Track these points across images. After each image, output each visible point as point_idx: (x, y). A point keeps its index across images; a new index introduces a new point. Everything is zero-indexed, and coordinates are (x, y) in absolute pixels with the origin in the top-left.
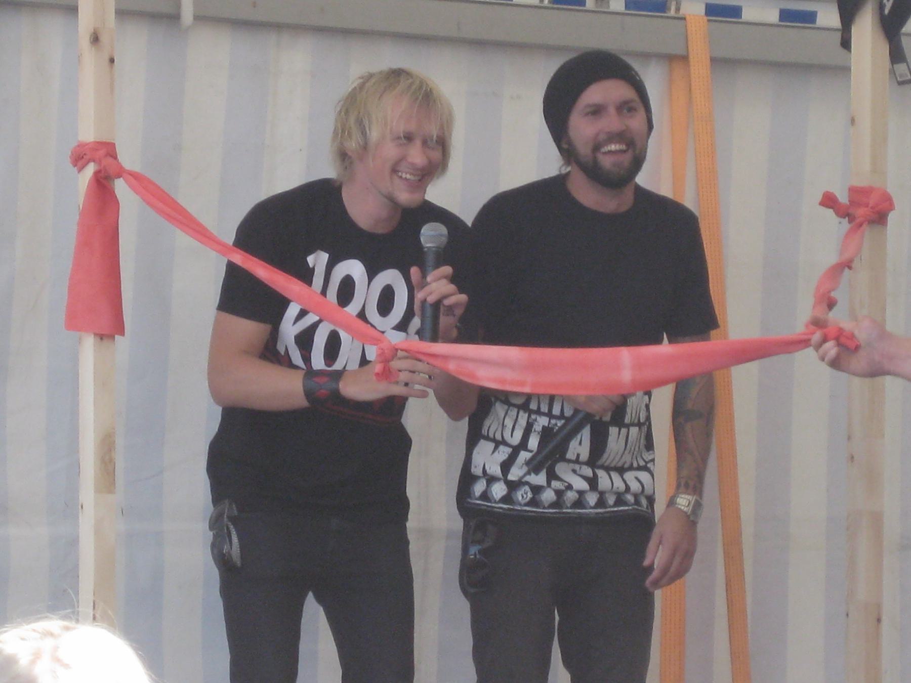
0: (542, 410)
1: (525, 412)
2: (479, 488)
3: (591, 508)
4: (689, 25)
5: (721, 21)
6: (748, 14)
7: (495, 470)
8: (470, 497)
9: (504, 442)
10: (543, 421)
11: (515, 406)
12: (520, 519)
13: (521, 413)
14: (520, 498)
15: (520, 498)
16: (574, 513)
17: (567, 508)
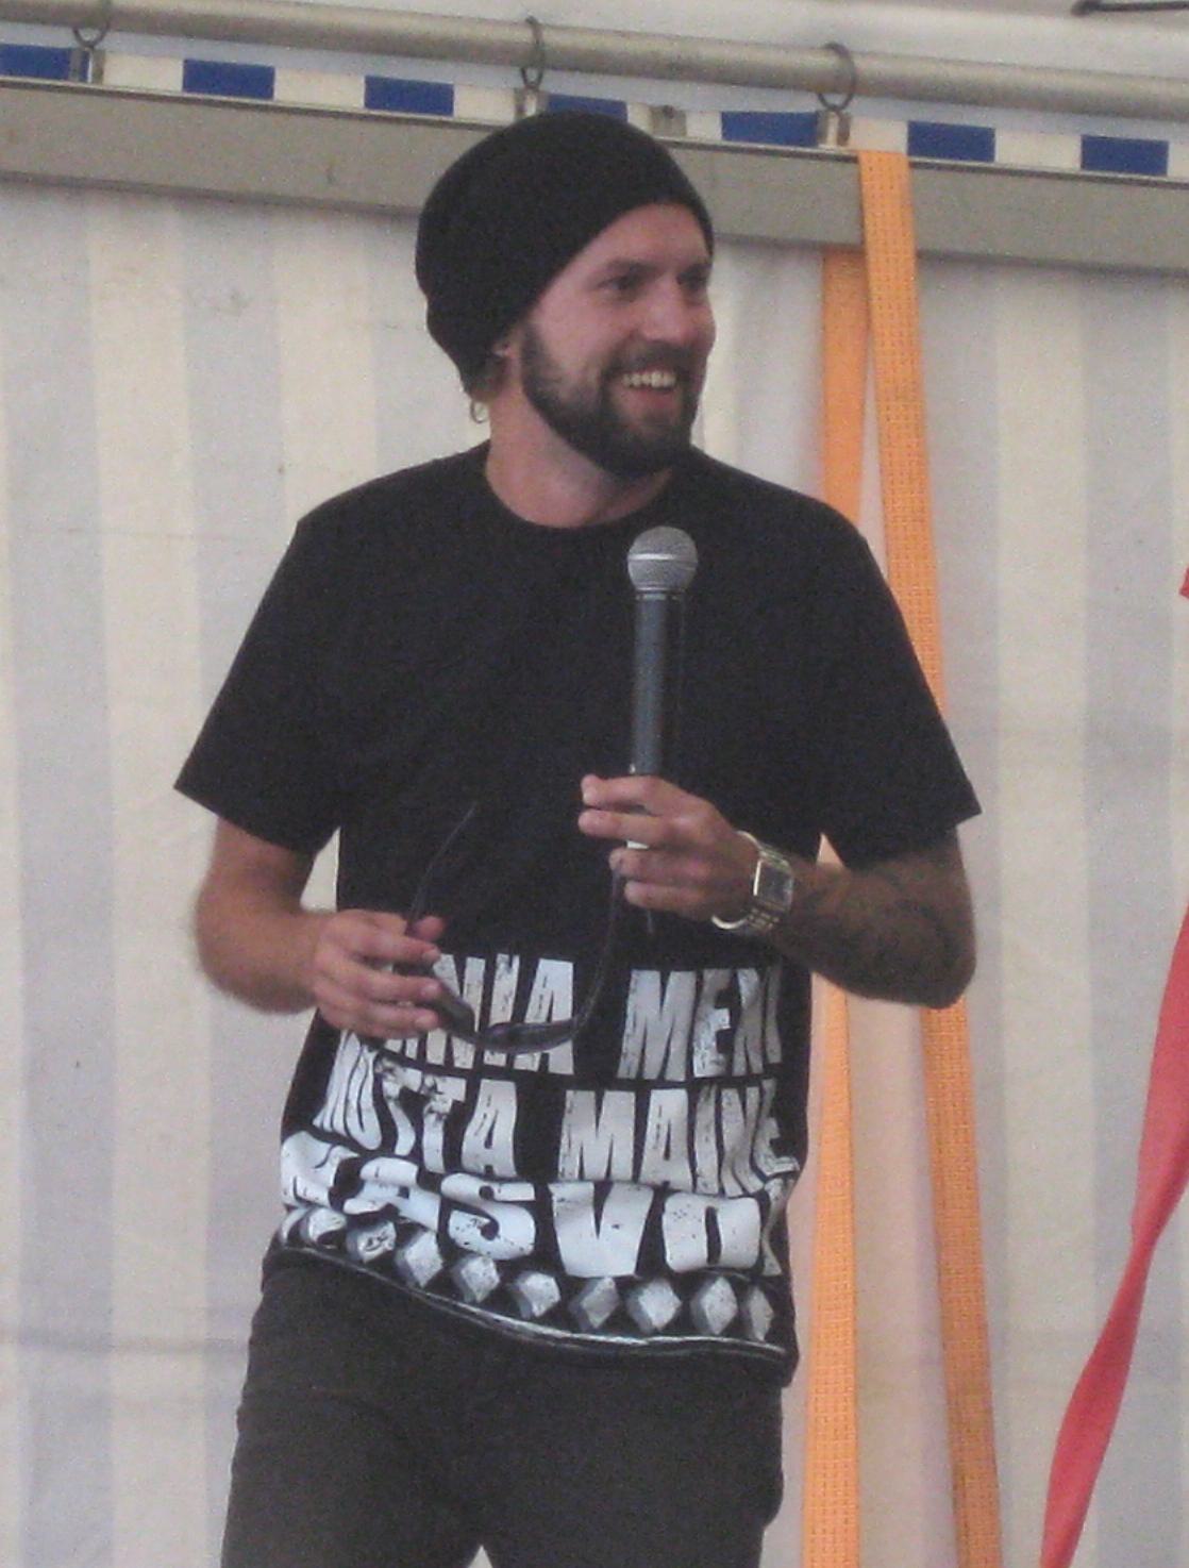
3: (533, 1319)
4: (866, 174)
5: (223, 104)
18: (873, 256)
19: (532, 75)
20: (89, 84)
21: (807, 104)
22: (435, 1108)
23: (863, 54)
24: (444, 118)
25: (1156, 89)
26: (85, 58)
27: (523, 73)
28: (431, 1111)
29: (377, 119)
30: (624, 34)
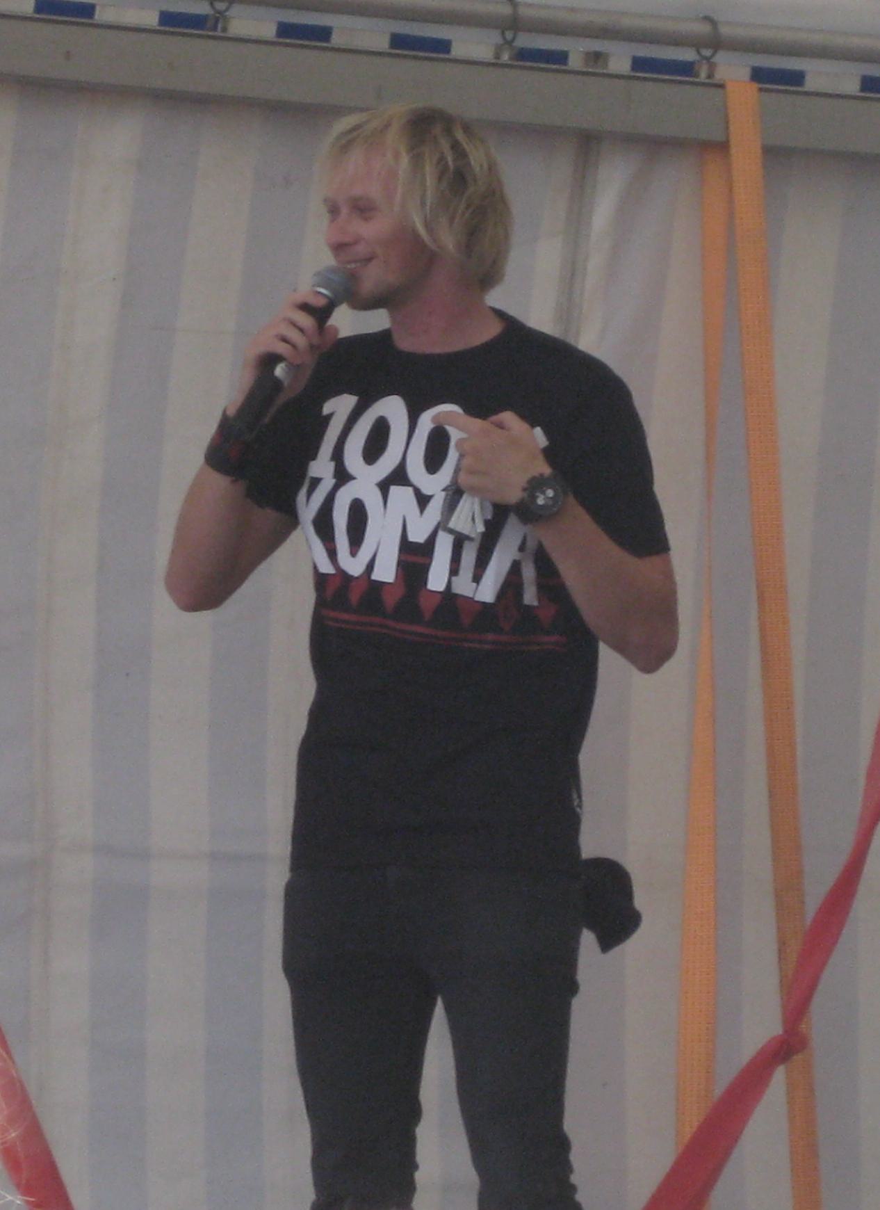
6: (101, 16)
18: (733, 151)
19: (509, 35)
20: (219, 33)
21: (688, 55)
24: (325, 45)
25: (856, 42)
26: (217, 20)
27: (503, 33)
29: (638, 78)
30: (573, 10)
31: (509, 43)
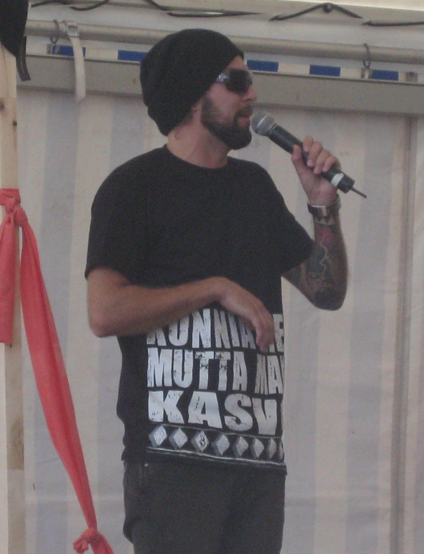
0: (205, 346)
1: (190, 351)
2: (159, 436)
7: (176, 416)
8: (151, 446)
9: (175, 387)
10: (209, 355)
11: (178, 348)
12: (174, 461)
13: (187, 352)
14: (199, 445)
15: (199, 445)
16: (245, 462)
17: (239, 457)
22: (203, 364)
23: (69, 21)
27: (364, 63)
28: (202, 366)
30: (328, 44)
31: (368, 67)
